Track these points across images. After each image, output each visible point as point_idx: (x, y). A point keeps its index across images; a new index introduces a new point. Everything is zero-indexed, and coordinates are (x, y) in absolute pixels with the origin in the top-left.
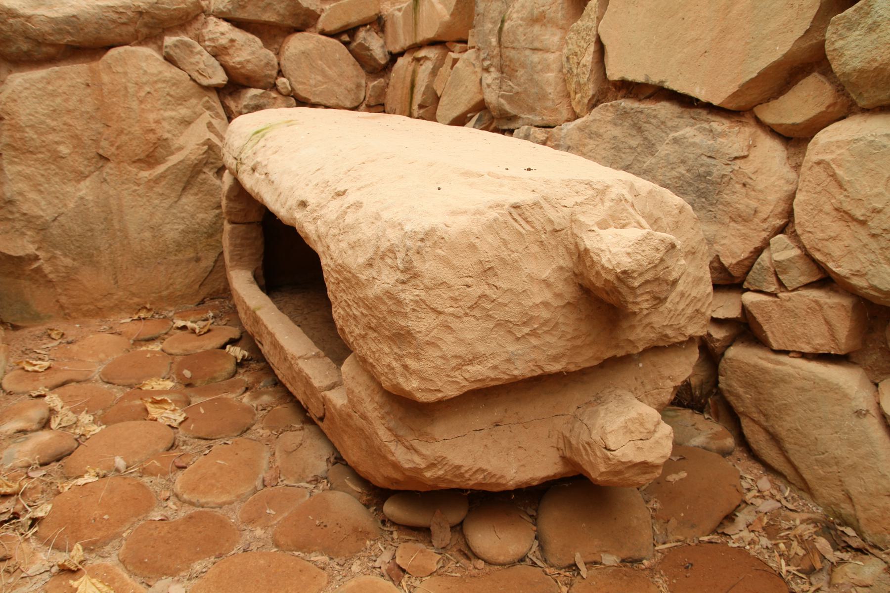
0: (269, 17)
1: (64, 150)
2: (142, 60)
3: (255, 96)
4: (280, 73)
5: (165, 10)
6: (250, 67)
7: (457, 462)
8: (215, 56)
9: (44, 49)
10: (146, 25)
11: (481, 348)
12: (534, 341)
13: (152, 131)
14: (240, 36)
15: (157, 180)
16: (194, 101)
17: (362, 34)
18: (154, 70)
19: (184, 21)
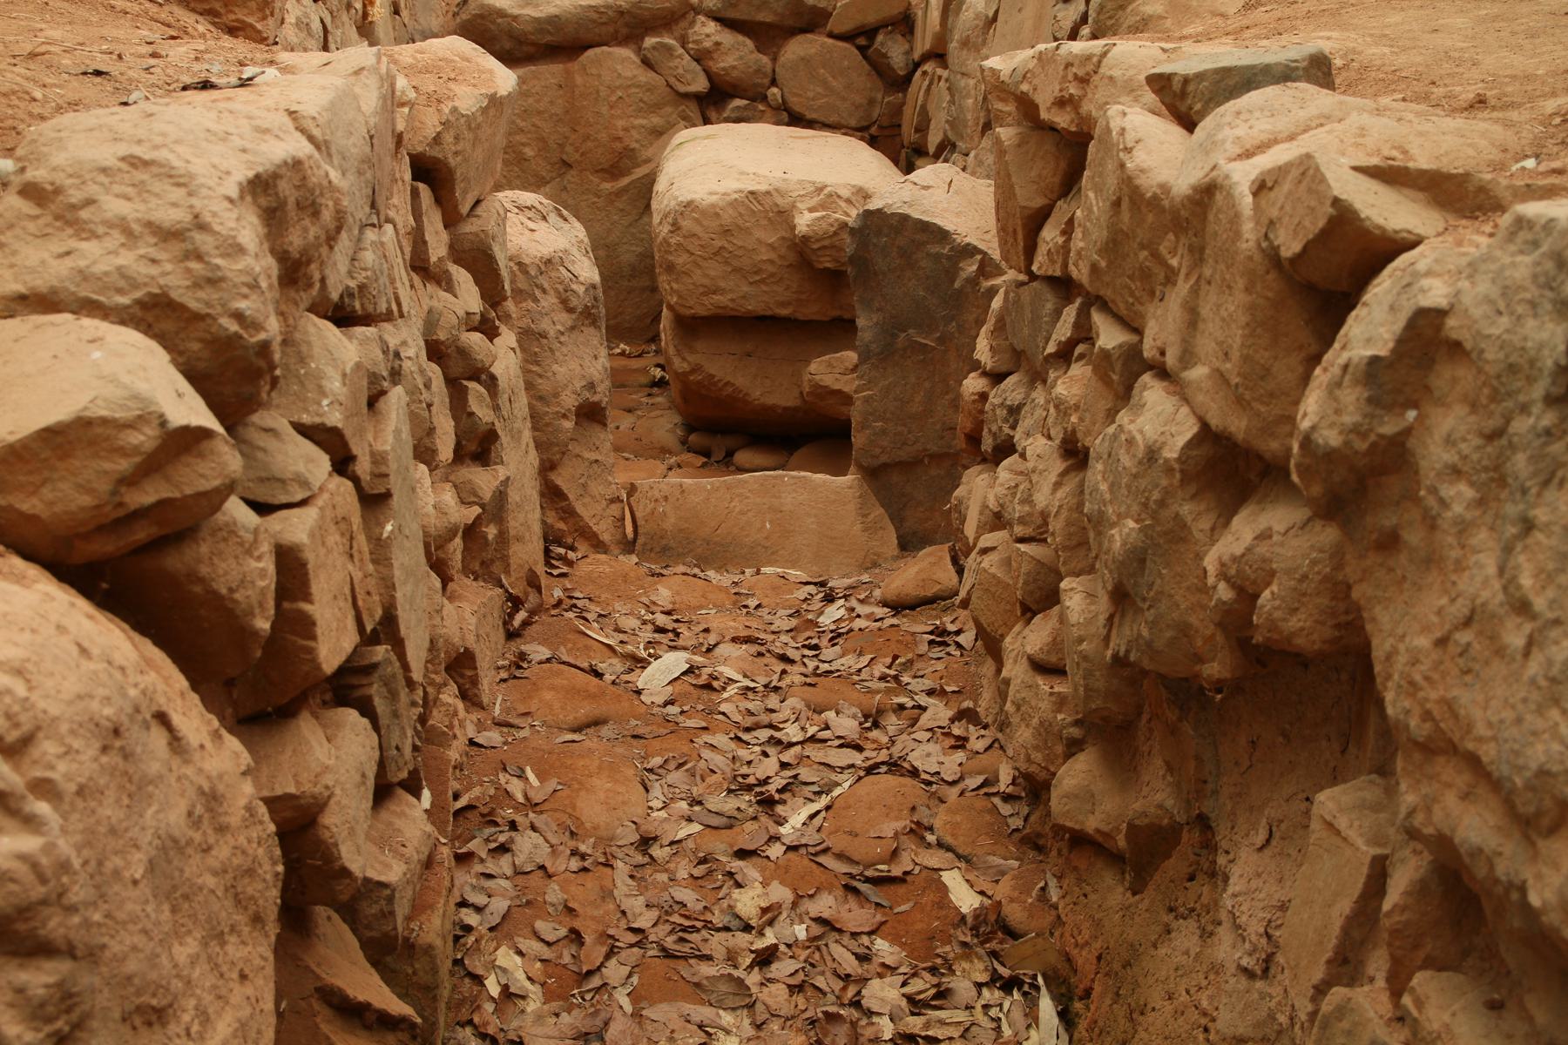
0: (765, 17)
1: (529, 152)
2: (620, 61)
3: (738, 107)
4: (774, 83)
5: (648, 9)
6: (735, 74)
7: (712, 371)
8: (697, 61)
9: (525, 48)
10: (627, 25)
11: (722, 284)
12: (764, 288)
13: (619, 139)
14: (727, 38)
15: (619, 193)
16: (669, 109)
17: (880, 38)
18: (629, 74)
19: (666, 21)
